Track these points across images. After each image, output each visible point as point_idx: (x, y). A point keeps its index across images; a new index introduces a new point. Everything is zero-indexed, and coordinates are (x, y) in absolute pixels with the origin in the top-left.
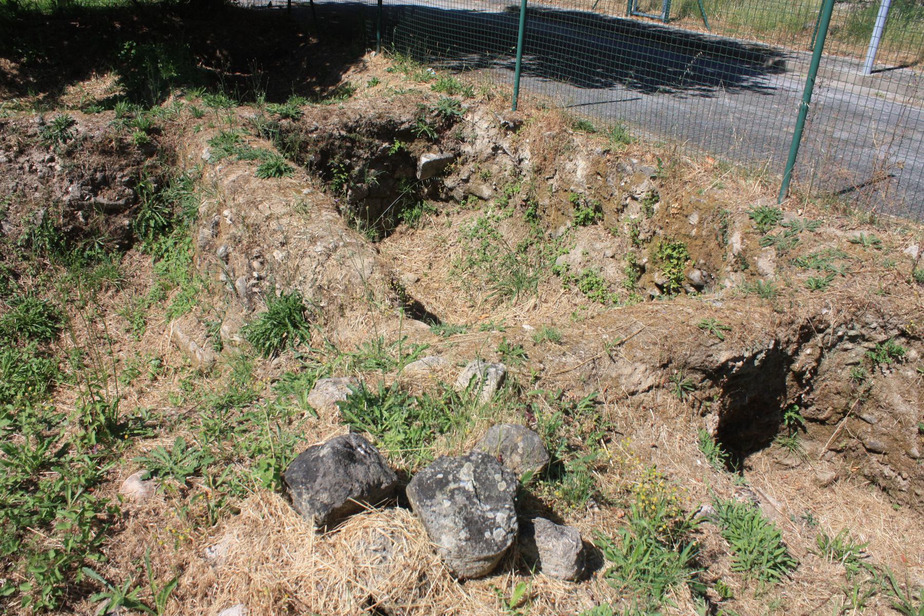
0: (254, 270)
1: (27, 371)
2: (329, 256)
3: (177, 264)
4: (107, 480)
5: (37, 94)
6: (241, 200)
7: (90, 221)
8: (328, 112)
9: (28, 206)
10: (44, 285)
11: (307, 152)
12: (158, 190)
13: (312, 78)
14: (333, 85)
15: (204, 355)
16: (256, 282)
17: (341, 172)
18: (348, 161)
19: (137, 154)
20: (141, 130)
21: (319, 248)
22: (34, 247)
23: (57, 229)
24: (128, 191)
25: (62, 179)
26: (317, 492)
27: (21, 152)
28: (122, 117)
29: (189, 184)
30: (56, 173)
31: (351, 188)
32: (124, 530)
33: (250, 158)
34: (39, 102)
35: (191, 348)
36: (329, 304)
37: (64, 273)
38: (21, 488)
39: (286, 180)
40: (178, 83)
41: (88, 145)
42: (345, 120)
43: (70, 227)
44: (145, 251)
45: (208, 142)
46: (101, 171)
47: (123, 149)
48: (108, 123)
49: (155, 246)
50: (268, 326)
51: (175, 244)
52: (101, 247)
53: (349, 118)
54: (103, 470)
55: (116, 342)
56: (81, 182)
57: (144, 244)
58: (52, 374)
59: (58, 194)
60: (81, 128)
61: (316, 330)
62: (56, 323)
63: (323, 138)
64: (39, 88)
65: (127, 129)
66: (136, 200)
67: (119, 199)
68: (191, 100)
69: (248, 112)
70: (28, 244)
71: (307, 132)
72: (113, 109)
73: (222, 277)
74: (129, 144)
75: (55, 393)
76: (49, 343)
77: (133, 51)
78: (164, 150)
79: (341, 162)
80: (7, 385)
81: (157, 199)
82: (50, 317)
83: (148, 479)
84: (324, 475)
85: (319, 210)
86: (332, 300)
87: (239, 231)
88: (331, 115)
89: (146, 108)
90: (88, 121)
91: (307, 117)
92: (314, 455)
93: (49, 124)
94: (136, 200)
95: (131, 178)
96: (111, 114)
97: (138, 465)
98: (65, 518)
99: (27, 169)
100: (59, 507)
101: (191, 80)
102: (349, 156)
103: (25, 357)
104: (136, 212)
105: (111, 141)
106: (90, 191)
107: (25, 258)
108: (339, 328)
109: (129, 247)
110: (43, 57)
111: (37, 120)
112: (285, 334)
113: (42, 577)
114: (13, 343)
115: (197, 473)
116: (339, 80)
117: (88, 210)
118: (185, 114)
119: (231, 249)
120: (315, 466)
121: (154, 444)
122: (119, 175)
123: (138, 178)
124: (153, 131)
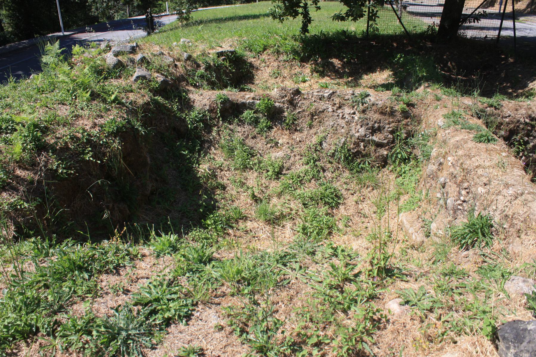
0: (462, 195)
1: (320, 221)
2: (516, 198)
3: (409, 181)
4: (379, 298)
5: (348, 78)
6: (460, 152)
7: (366, 149)
8: (519, 106)
9: (337, 136)
10: (336, 178)
11: (500, 129)
12: (406, 138)
13: (507, 83)
14: (522, 89)
15: (418, 237)
16: (461, 203)
17: (520, 144)
18: (526, 139)
19: (399, 116)
20: (404, 104)
21: (511, 191)
22: (335, 157)
23: (349, 150)
24: (390, 136)
25: (357, 124)
26: (521, 351)
27: (340, 107)
28: (395, 95)
29: (426, 137)
30: (355, 121)
31: (525, 156)
32: (386, 329)
33: (469, 128)
34: (349, 82)
35: (410, 231)
36: (510, 227)
37: (347, 174)
38: (335, 288)
39: (491, 146)
40: (427, 79)
41: (374, 108)
42: (530, 112)
43: (356, 150)
44: (392, 170)
45: (443, 115)
46: (378, 123)
47: (392, 113)
48: (387, 97)
49: (398, 169)
50: (467, 231)
51: (410, 170)
52: (369, 164)
53: (533, 112)
54: (378, 292)
55: (367, 217)
56: (366, 127)
57: (392, 167)
58: (332, 226)
59: (354, 132)
60: (372, 99)
61: (497, 241)
62: (339, 199)
63: (512, 122)
64: (349, 75)
65: (396, 102)
66: (393, 142)
67: (384, 140)
68: (434, 90)
69: (467, 101)
70: (333, 155)
71: (502, 117)
72: (390, 90)
73: (439, 195)
74: (396, 111)
75: (331, 237)
76: (333, 210)
77: (402, 59)
78: (415, 116)
79: (522, 138)
80: (310, 226)
81: (404, 143)
82: (336, 196)
83: (403, 305)
84: (529, 342)
85: (512, 168)
86: (512, 225)
87: (457, 171)
88: (521, 108)
89: (408, 92)
90: (377, 95)
91: (505, 108)
92: (522, 326)
93: (356, 95)
94: (393, 142)
95: (394, 129)
96: (389, 93)
97: (397, 295)
98: (357, 311)
99: (341, 116)
100: (353, 305)
101: (433, 78)
102: (528, 135)
103: (320, 214)
104: (391, 148)
105: (386, 108)
106: (371, 133)
107: (331, 163)
108: (515, 244)
109: (384, 167)
110: (354, 60)
111: (351, 92)
112: (476, 239)
113: (345, 340)
114: (316, 205)
115: (431, 310)
116: (526, 86)
117: (367, 143)
118: (430, 97)
119: (448, 180)
120: (523, 334)
121: (407, 285)
122: (387, 126)
123: (397, 130)
124: (410, 105)
